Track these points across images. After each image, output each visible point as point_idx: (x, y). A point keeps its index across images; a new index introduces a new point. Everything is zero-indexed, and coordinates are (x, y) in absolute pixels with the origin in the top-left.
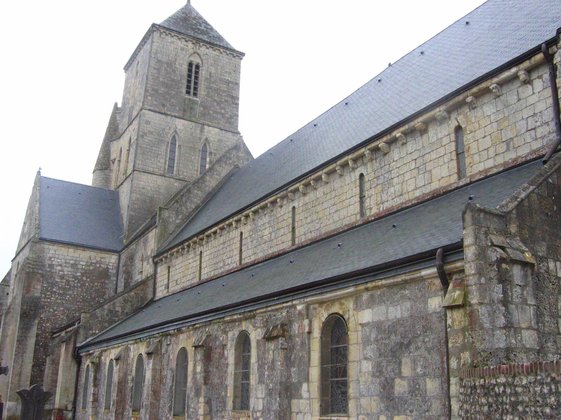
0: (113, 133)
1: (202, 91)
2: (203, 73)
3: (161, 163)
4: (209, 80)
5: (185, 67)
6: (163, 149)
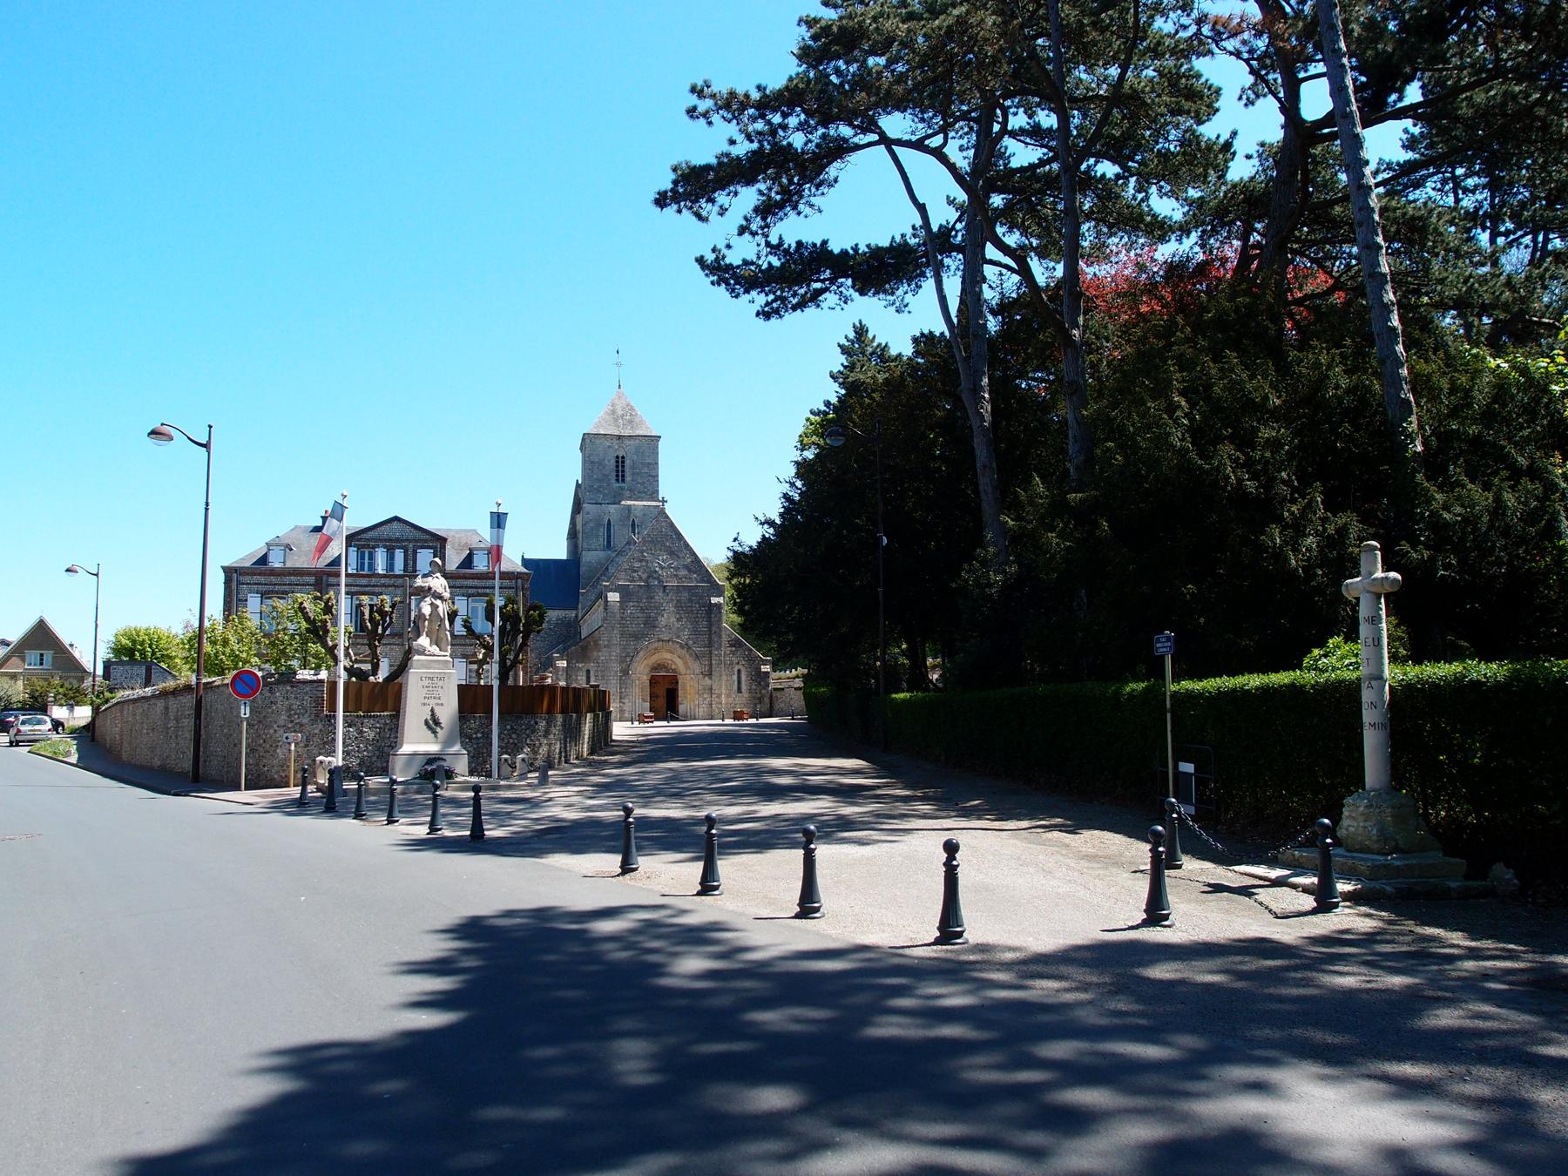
0: (577, 507)
1: (628, 478)
2: (628, 462)
3: (602, 541)
4: (633, 467)
5: (613, 461)
6: (602, 532)
